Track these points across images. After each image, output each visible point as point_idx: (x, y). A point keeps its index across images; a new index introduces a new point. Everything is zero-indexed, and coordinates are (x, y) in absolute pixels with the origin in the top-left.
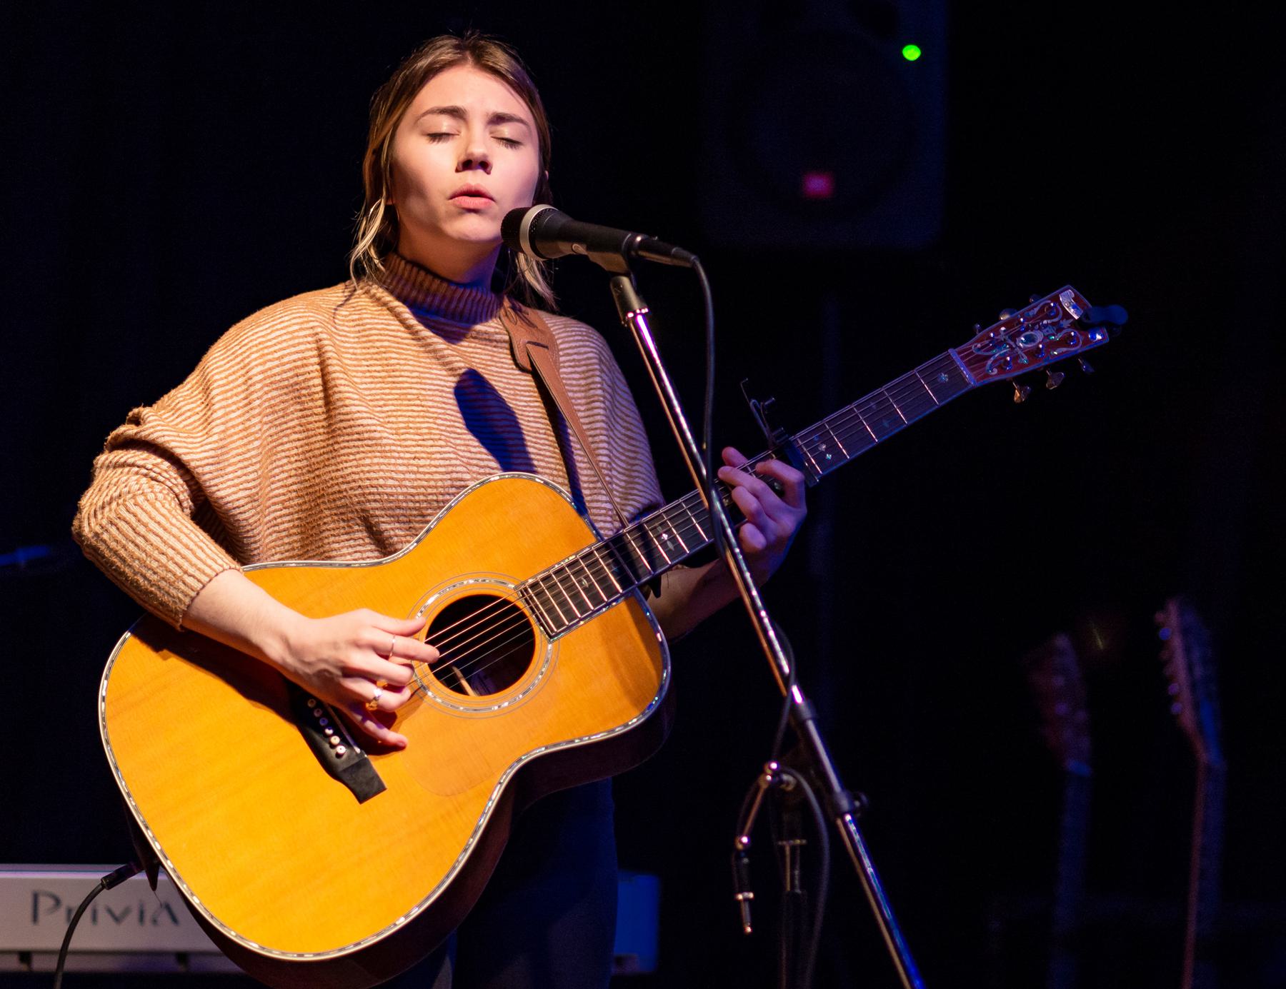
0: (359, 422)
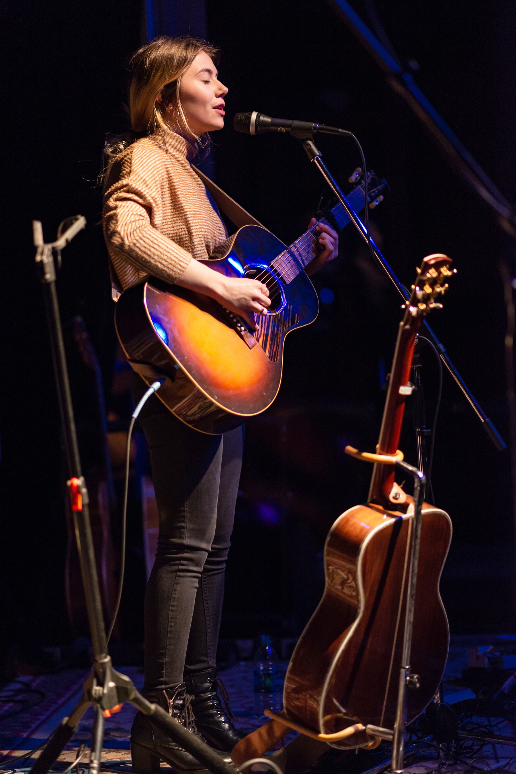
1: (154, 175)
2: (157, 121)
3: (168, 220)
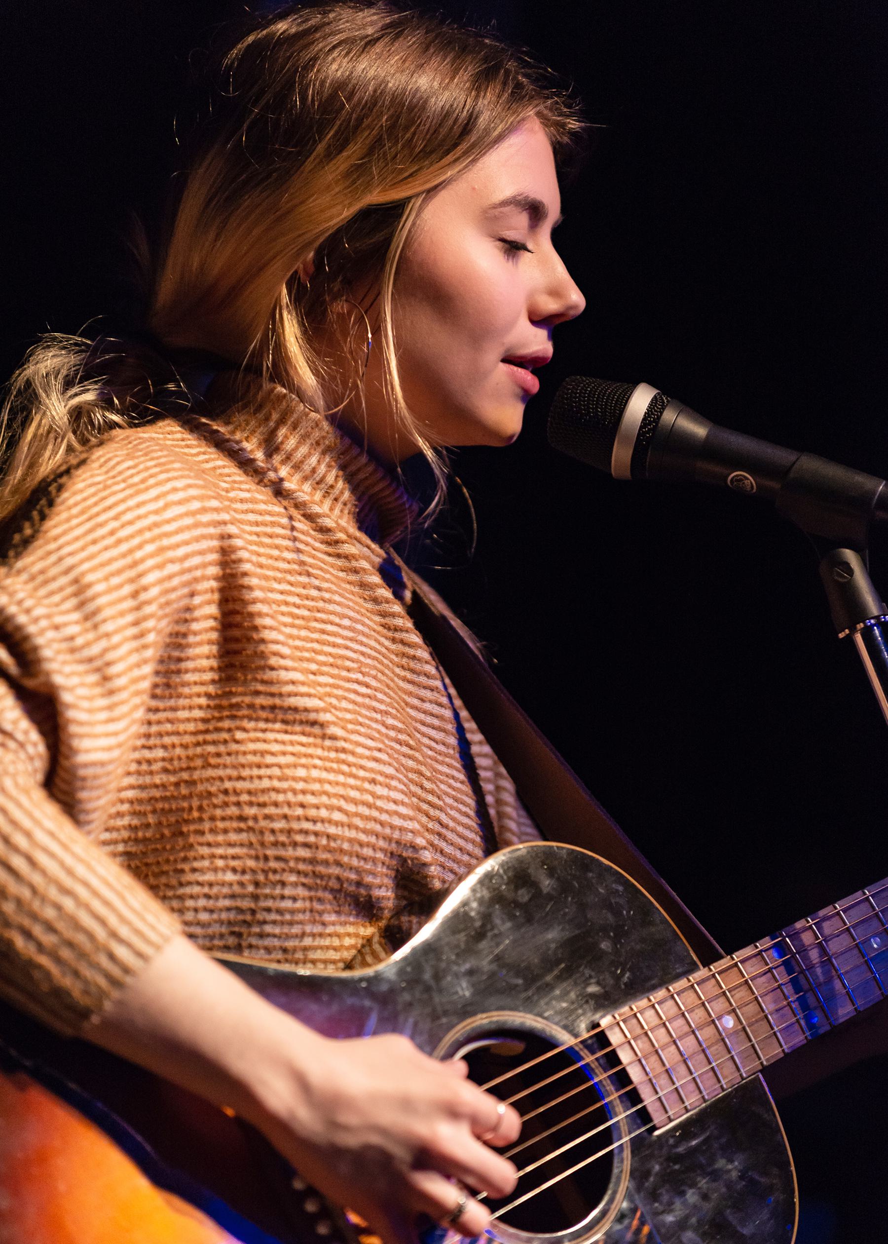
1: (135, 564)
2: (280, 347)
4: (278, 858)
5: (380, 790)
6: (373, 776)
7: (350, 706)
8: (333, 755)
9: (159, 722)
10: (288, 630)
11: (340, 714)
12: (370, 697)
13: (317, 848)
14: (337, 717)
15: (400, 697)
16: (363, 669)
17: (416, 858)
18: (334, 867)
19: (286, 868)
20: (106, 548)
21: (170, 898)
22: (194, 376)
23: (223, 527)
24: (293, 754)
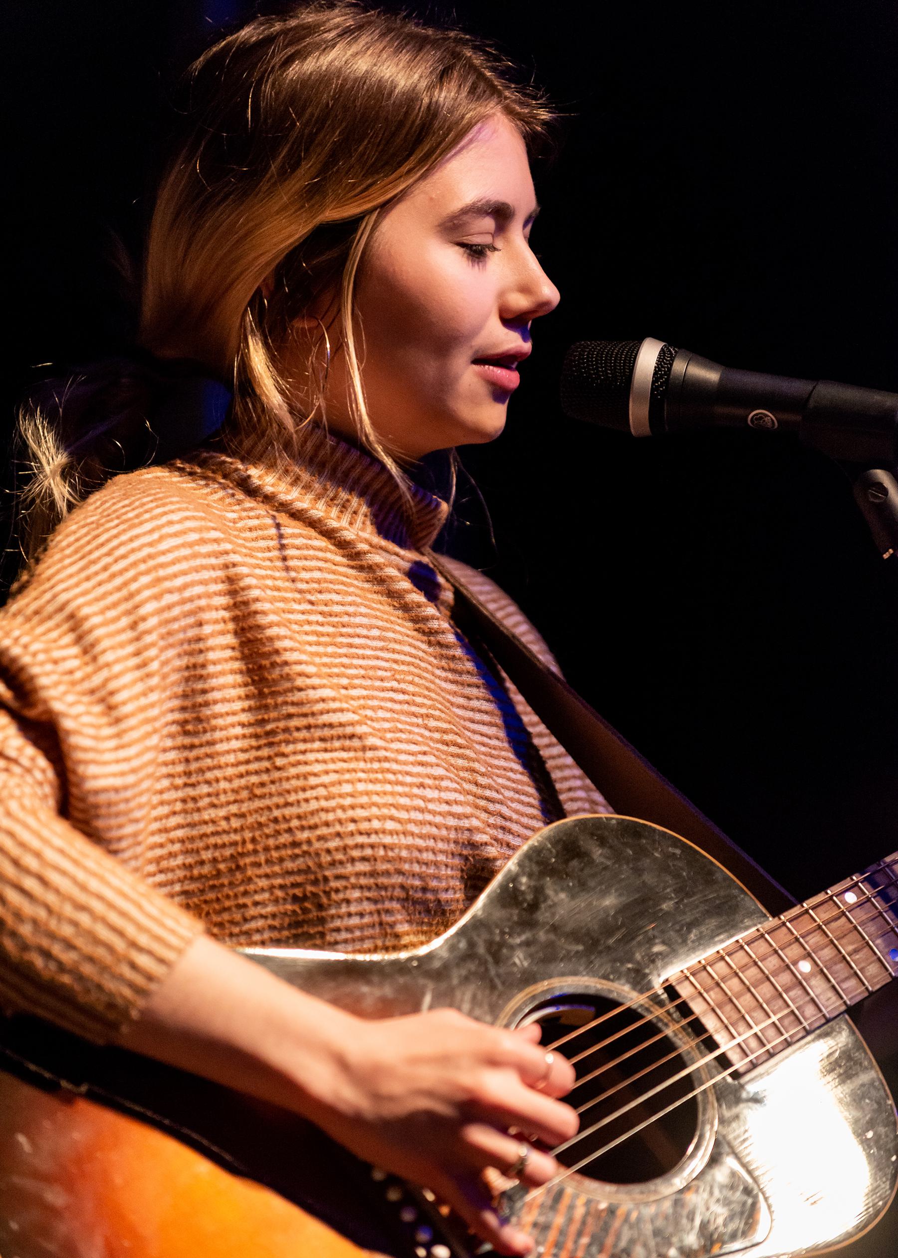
0: (325, 718)
1: (131, 596)
3: (223, 785)
4: (338, 877)
5: (430, 794)
6: (421, 780)
7: (388, 715)
8: (376, 765)
9: (197, 759)
10: (314, 649)
11: (376, 725)
12: (408, 703)
13: (375, 860)
14: (374, 729)
15: (443, 698)
16: (398, 677)
17: (478, 855)
18: (396, 876)
19: (348, 885)
20: (100, 584)
21: (237, 935)
22: (182, 417)
23: (225, 557)
24: (336, 772)
